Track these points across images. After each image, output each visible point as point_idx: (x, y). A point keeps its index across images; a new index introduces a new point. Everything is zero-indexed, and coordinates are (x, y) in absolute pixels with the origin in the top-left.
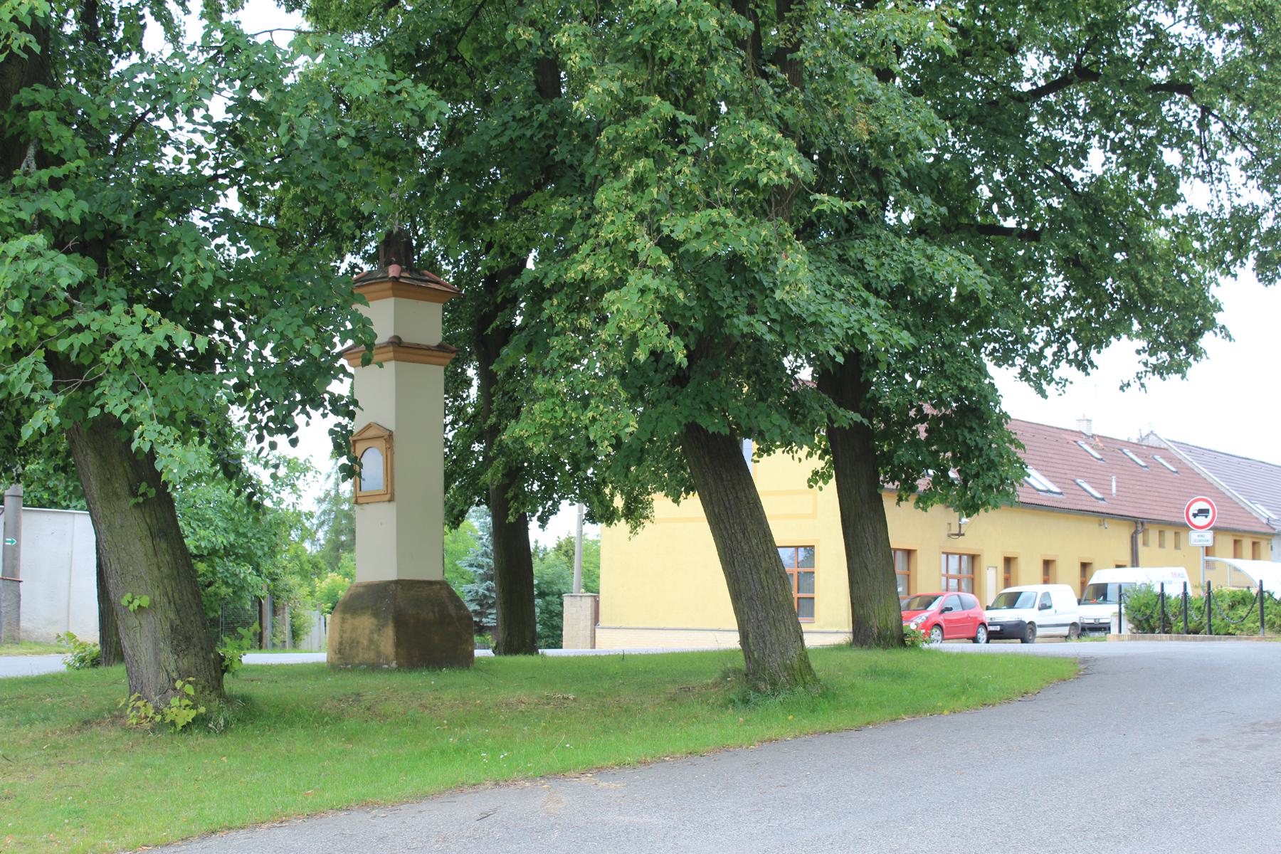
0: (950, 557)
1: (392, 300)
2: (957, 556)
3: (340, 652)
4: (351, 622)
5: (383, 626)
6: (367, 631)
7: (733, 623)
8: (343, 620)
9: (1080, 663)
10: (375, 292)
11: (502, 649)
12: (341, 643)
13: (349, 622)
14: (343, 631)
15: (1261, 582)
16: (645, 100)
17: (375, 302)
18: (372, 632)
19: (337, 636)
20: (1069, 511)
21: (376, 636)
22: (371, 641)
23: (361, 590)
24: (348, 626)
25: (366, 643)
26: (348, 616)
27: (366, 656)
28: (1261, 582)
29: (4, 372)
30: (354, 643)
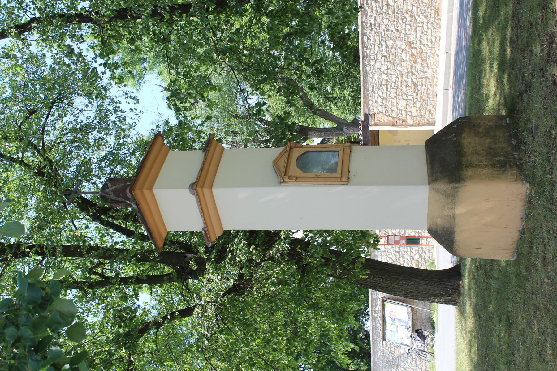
0: (389, 243)
2: (389, 243)
3: (502, 167)
7: (440, 269)
8: (470, 165)
11: (454, 296)
12: (493, 166)
13: (469, 158)
14: (479, 166)
15: (161, 92)
16: (187, 255)
17: (223, 227)
18: (477, 134)
19: (485, 171)
21: (481, 130)
22: (486, 134)
24: (474, 161)
25: (488, 140)
28: (161, 92)
30: (491, 153)
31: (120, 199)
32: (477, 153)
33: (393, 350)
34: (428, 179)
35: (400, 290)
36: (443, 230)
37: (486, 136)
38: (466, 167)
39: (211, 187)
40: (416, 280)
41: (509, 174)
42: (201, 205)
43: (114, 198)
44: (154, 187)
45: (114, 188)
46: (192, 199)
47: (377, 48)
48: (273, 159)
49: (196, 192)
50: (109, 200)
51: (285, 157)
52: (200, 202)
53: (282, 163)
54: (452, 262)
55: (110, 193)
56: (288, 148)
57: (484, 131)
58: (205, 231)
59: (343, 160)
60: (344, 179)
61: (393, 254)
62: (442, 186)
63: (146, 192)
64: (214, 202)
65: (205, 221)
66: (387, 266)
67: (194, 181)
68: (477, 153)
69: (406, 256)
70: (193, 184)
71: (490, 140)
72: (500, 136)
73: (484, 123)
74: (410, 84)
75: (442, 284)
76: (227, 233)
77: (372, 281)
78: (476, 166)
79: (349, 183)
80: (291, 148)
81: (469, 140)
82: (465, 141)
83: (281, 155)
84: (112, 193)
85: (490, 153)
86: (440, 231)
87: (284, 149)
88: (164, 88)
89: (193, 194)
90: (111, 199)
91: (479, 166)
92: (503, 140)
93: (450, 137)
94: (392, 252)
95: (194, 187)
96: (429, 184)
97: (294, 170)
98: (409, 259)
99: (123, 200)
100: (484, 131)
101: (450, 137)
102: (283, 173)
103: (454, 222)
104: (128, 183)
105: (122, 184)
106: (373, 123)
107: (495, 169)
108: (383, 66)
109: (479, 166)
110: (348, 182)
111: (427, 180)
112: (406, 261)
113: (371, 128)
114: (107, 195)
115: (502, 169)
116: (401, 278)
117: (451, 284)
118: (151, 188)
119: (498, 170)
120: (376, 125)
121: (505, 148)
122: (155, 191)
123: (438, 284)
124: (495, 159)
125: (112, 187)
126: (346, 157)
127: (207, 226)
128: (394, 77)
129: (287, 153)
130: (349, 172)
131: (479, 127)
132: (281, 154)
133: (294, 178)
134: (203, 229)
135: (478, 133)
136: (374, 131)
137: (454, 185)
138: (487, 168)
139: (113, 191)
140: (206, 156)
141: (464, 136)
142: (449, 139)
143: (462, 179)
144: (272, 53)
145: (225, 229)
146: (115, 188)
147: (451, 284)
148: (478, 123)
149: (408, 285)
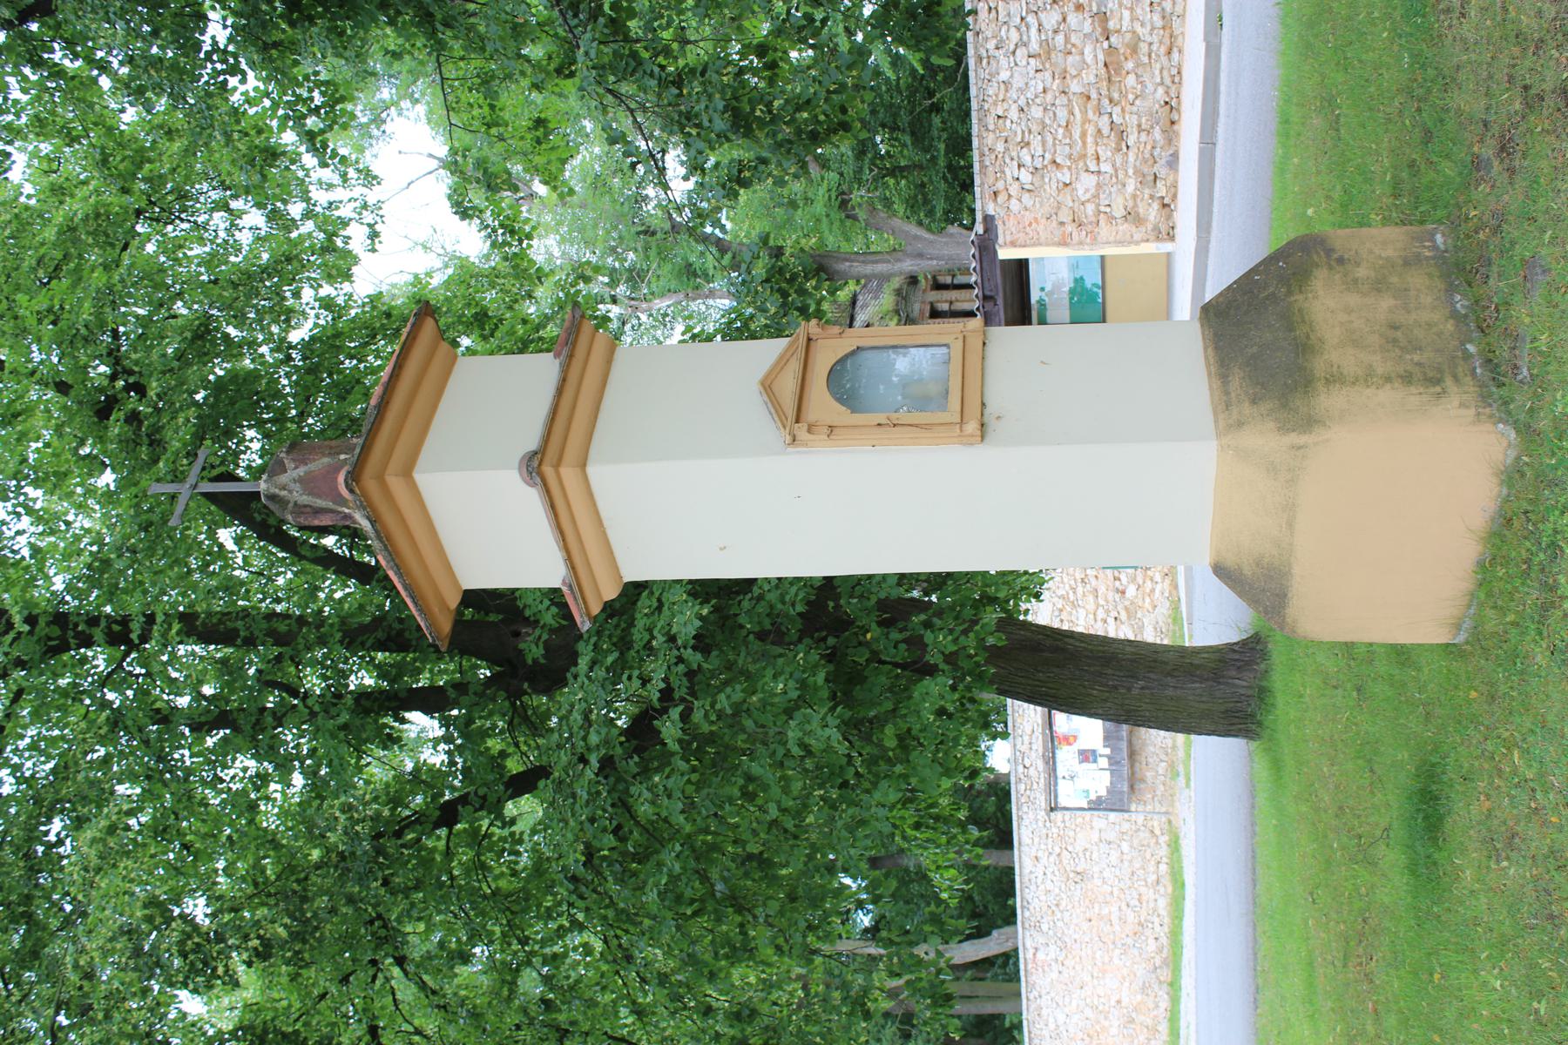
1: (596, 472)
3: (1437, 381)
4: (1335, 355)
5: (1329, 252)
6: (1353, 299)
8: (1335, 379)
9: (1253, 797)
10: (589, 354)
12: (1407, 379)
14: (1368, 378)
18: (1353, 284)
20: (983, 369)
21: (1361, 272)
22: (1379, 285)
23: (1235, 382)
25: (1386, 303)
26: (1319, 366)
27: (1427, 300)
29: (697, 6)
30: (1395, 337)
31: (320, 503)
33: (1071, 834)
34: (1216, 422)
35: (1108, 704)
36: (1258, 565)
37: (1379, 291)
39: (583, 465)
40: (1152, 676)
41: (1456, 403)
42: (556, 515)
43: (305, 499)
44: (417, 468)
45: (301, 471)
46: (532, 498)
47: (1014, 36)
48: (760, 375)
49: (538, 480)
50: (291, 505)
51: (795, 366)
52: (553, 506)
53: (788, 385)
55: (292, 486)
56: (802, 341)
57: (1372, 274)
58: (570, 587)
60: (972, 427)
61: (1067, 587)
62: (1264, 439)
63: (395, 484)
64: (612, 553)
65: (569, 559)
66: (1071, 641)
67: (533, 444)
69: (1102, 590)
71: (1392, 302)
72: (1418, 290)
73: (1371, 252)
74: (1106, 131)
75: (1219, 683)
76: (635, 590)
77: (1030, 682)
79: (990, 436)
80: (809, 340)
83: (781, 363)
84: (297, 487)
85: (1395, 341)
86: (1247, 571)
87: (790, 345)
88: (440, 160)
89: (534, 485)
90: (296, 503)
91: (1366, 381)
92: (1429, 300)
94: (1065, 580)
95: (535, 466)
96: (1219, 435)
97: (821, 401)
98: (1110, 598)
99: (330, 505)
100: (1372, 274)
102: (791, 413)
103: (1291, 544)
104: (342, 457)
105: (326, 460)
106: (1009, 238)
107: (1413, 389)
108: (1033, 82)
109: (1366, 381)
110: (983, 437)
111: (1212, 425)
112: (1102, 602)
113: (1005, 254)
114: (283, 493)
116: (1110, 671)
117: (1244, 684)
118: (407, 472)
119: (1422, 390)
120: (1013, 244)
122: (420, 477)
123: (1210, 683)
124: (1408, 357)
125: (296, 468)
127: (575, 573)
128: (1062, 114)
129: (801, 353)
130: (983, 404)
131: (1358, 264)
132: (781, 357)
133: (825, 430)
134: (564, 583)
135: (1356, 281)
136: (1010, 261)
137: (1294, 438)
138: (1388, 386)
139: (300, 480)
140: (547, 491)
143: (1316, 422)
145: (627, 579)
146: (306, 473)
147: (1244, 684)
148: (1353, 253)
149: (1129, 689)
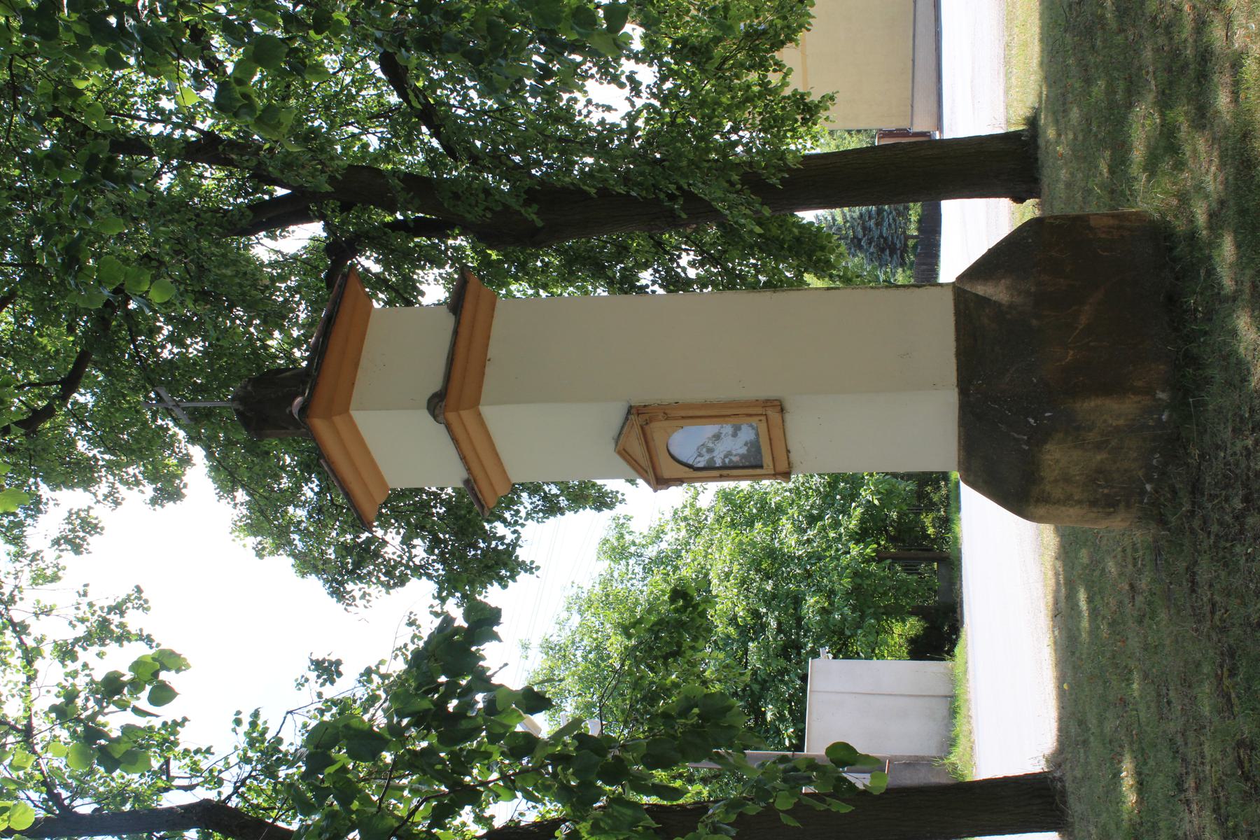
12: (1093, 503)
13: (1048, 488)
24: (1057, 493)
32: (1067, 479)
38: (1037, 501)
54: (1001, 119)
59: (770, 439)
67: (436, 385)
68: (1067, 479)
70: (435, 396)
78: (1058, 502)
81: (1057, 455)
82: (1048, 457)
93: (1016, 435)
95: (438, 404)
101: (1016, 435)
115: (1108, 510)
121: (1103, 28)
126: (777, 433)
130: (788, 451)
141: (1048, 447)
142: (1015, 439)
144: (628, 28)
